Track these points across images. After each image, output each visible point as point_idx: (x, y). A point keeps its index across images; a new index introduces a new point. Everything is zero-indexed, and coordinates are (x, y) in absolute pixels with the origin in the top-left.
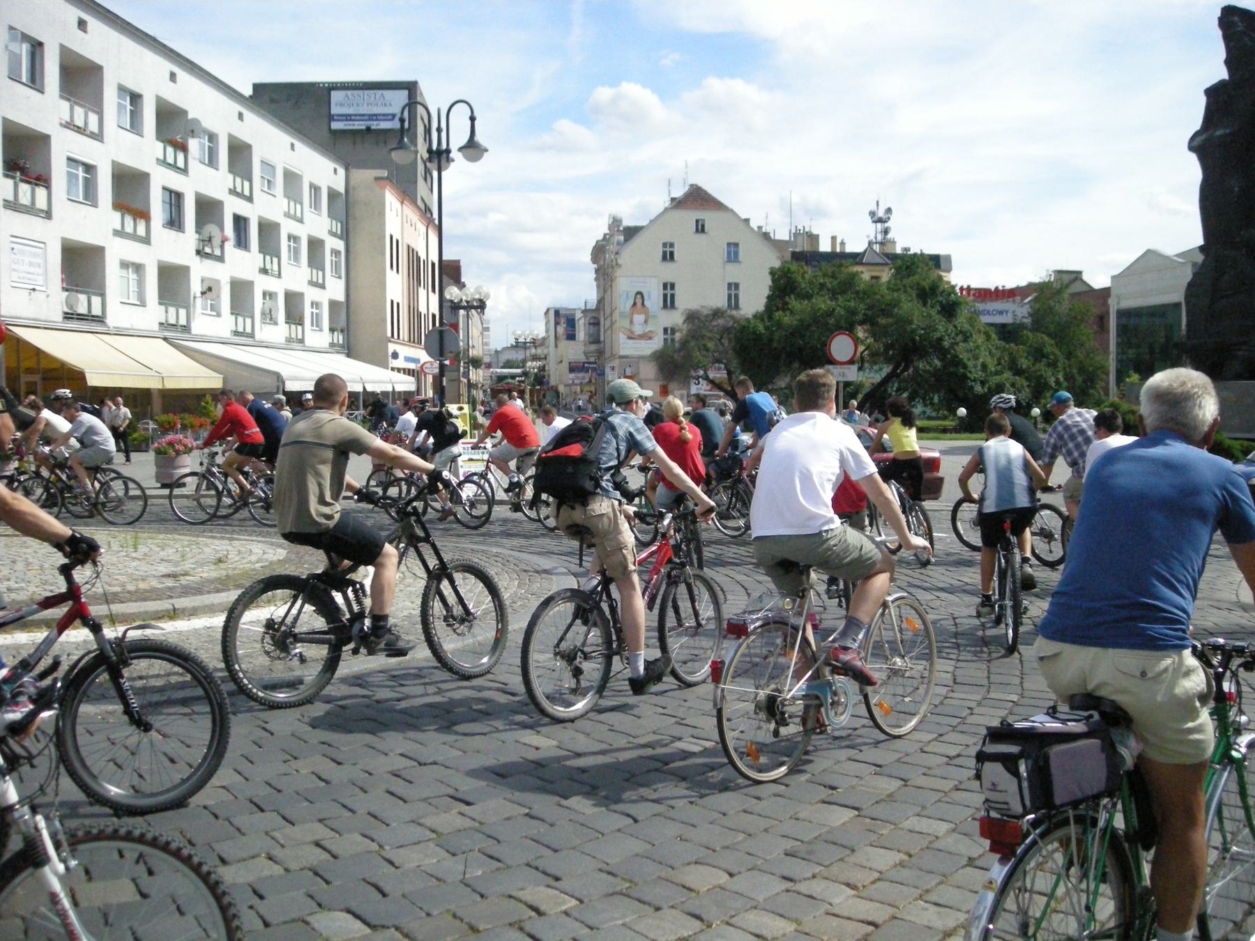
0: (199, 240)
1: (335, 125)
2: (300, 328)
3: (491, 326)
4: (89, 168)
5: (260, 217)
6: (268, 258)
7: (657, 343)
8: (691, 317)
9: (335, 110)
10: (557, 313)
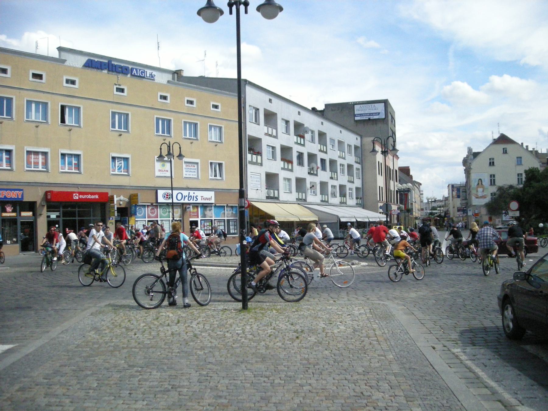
0: (309, 169)
1: (357, 118)
2: (345, 198)
3: (424, 193)
4: (273, 148)
5: (330, 159)
6: (333, 173)
7: (488, 200)
8: (500, 189)
9: (356, 112)
10: (453, 186)
